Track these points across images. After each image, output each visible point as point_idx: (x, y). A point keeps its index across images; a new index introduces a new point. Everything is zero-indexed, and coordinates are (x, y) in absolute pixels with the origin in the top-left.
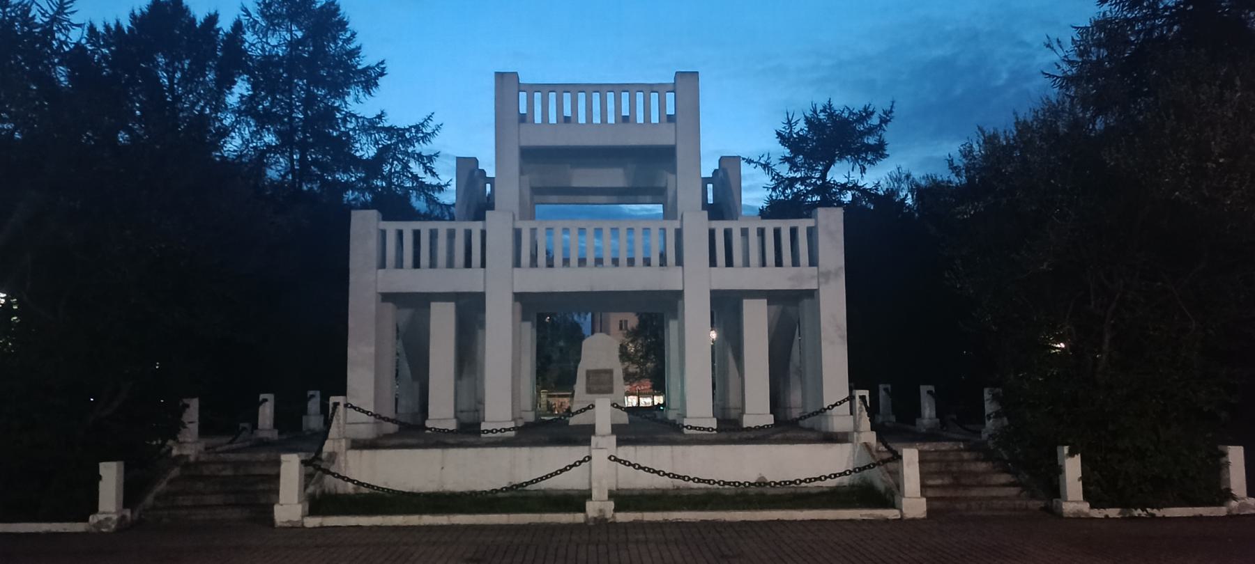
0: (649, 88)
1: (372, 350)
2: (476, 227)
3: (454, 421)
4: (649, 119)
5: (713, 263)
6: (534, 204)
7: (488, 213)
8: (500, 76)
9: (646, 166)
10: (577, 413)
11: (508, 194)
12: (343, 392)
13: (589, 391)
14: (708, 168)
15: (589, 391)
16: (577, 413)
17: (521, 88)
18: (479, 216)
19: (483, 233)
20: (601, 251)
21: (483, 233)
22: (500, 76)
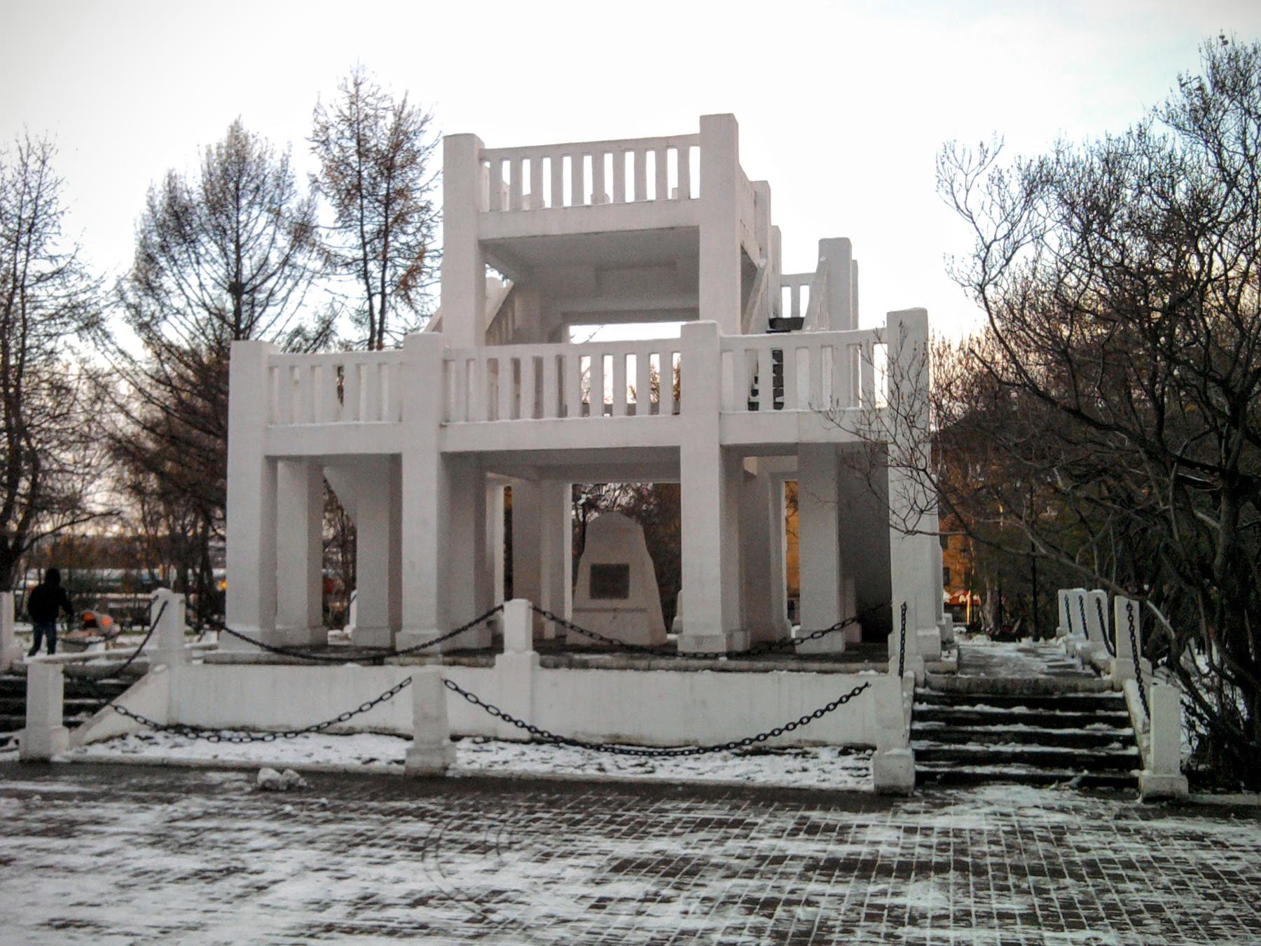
0: (661, 145)
17: (484, 155)
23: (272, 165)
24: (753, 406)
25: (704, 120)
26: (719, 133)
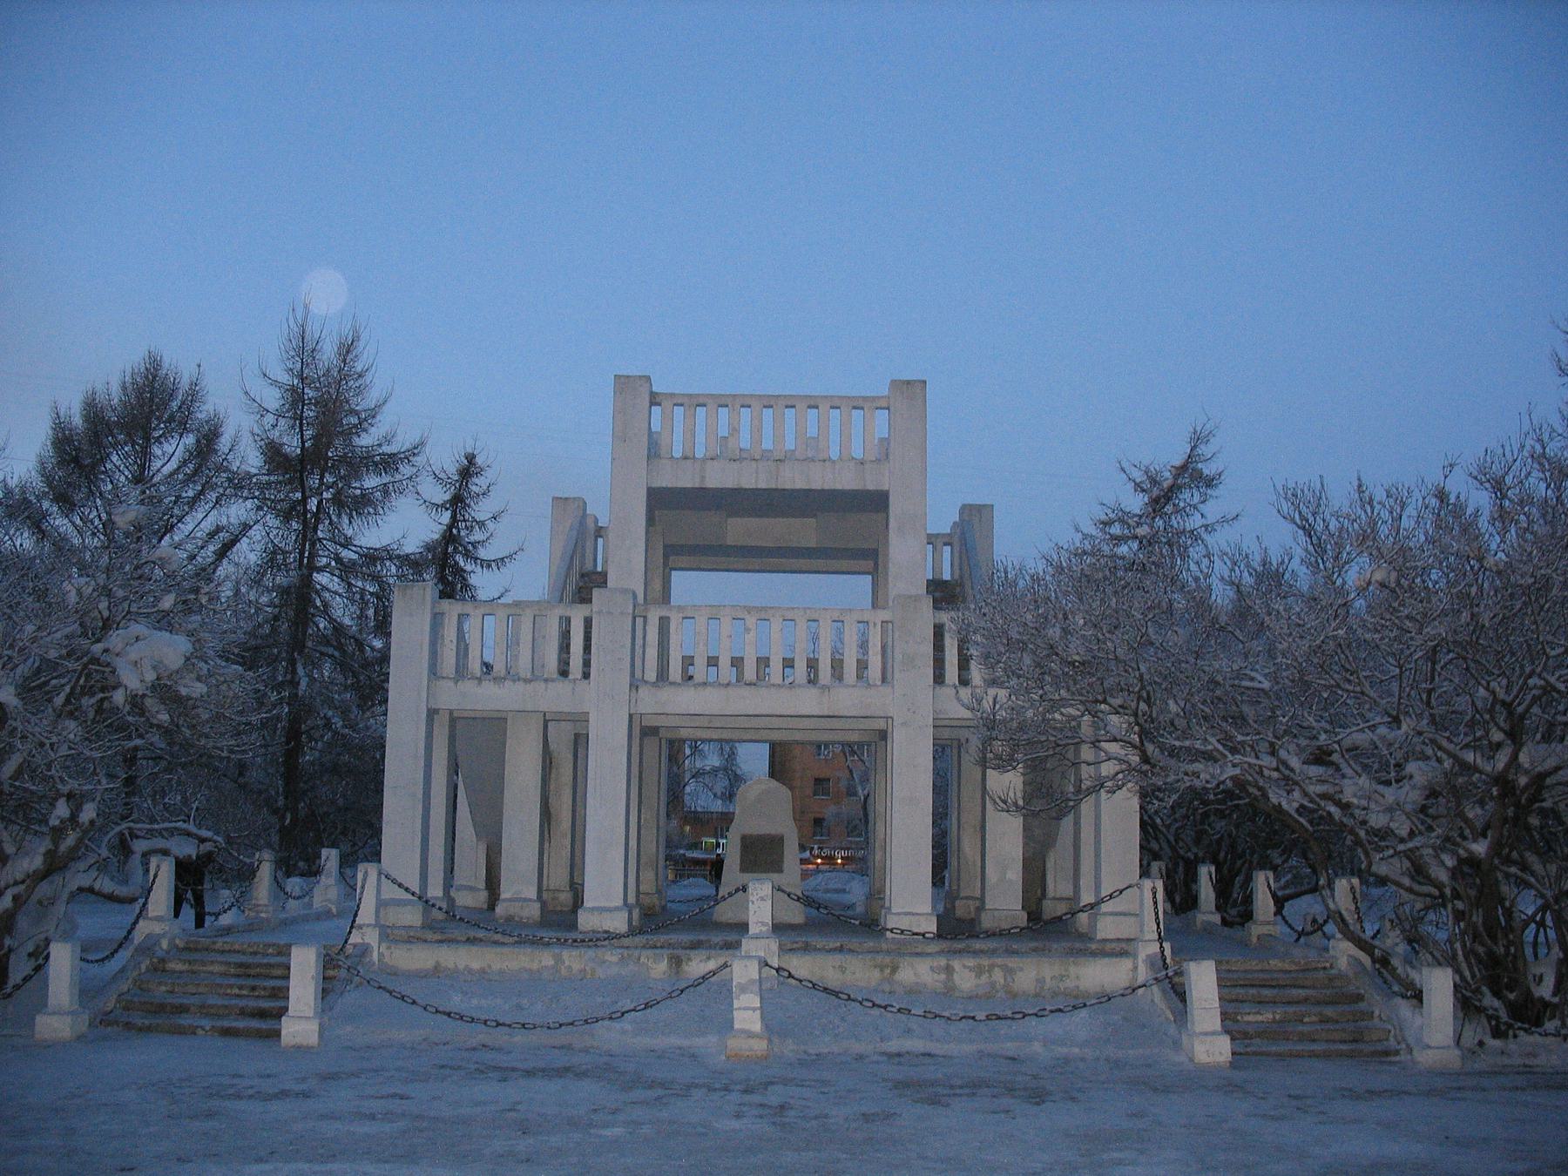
1: (812, 544)
2: (577, 615)
3: (537, 905)
4: (839, 455)
5: (939, 678)
6: (668, 569)
7: (596, 592)
8: (624, 384)
9: (835, 526)
10: (991, 934)
11: (626, 559)
12: (376, 856)
13: (744, 869)
14: (943, 519)
15: (744, 869)
16: (991, 934)
17: (654, 400)
18: (583, 596)
19: (588, 623)
20: (765, 649)
21: (588, 623)
22: (624, 384)
23: (184, 385)
24: (564, 673)
25: (895, 384)
26: (911, 390)
